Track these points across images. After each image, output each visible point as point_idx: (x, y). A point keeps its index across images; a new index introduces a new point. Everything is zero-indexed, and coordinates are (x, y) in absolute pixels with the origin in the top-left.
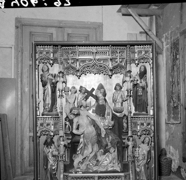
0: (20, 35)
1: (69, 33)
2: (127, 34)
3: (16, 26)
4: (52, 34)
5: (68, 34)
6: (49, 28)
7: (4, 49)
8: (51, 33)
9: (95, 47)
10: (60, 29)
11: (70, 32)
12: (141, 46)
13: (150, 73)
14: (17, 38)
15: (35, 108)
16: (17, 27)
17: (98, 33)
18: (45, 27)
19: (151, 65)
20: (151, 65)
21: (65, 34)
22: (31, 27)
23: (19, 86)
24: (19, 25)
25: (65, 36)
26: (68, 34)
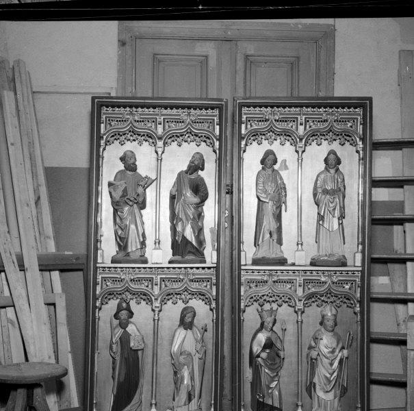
0: (130, 62)
1: (249, 53)
2: (400, 51)
3: (119, 41)
4: (206, 57)
5: (247, 57)
6: (198, 44)
7: (68, 96)
8: (204, 54)
9: (186, 110)
10: (227, 45)
11: (252, 52)
12: (319, 108)
13: (84, 215)
14: (122, 70)
15: (366, 158)
16: (122, 43)
17: (323, 53)
18: (189, 41)
19: (361, 152)
20: (361, 152)
21: (238, 58)
22: (156, 41)
23: (38, 173)
24: (126, 37)
25: (238, 62)
26: (247, 57)
